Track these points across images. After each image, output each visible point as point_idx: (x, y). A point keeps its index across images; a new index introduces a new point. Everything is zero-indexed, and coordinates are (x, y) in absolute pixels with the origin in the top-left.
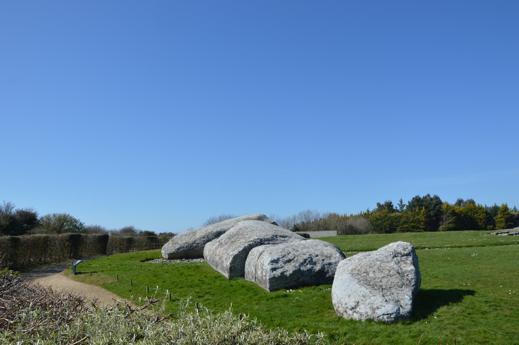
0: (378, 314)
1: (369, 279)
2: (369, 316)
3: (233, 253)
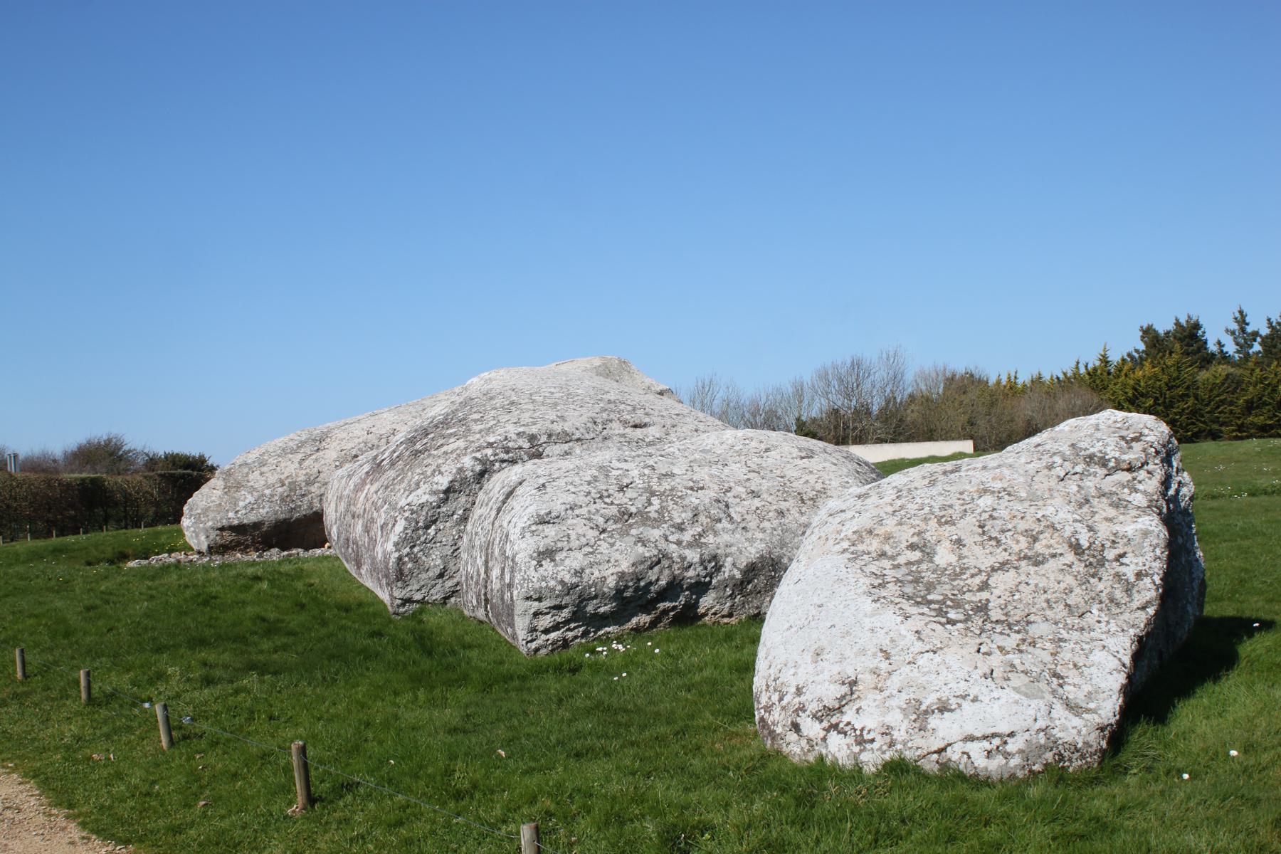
1: (929, 576)
2: (899, 747)
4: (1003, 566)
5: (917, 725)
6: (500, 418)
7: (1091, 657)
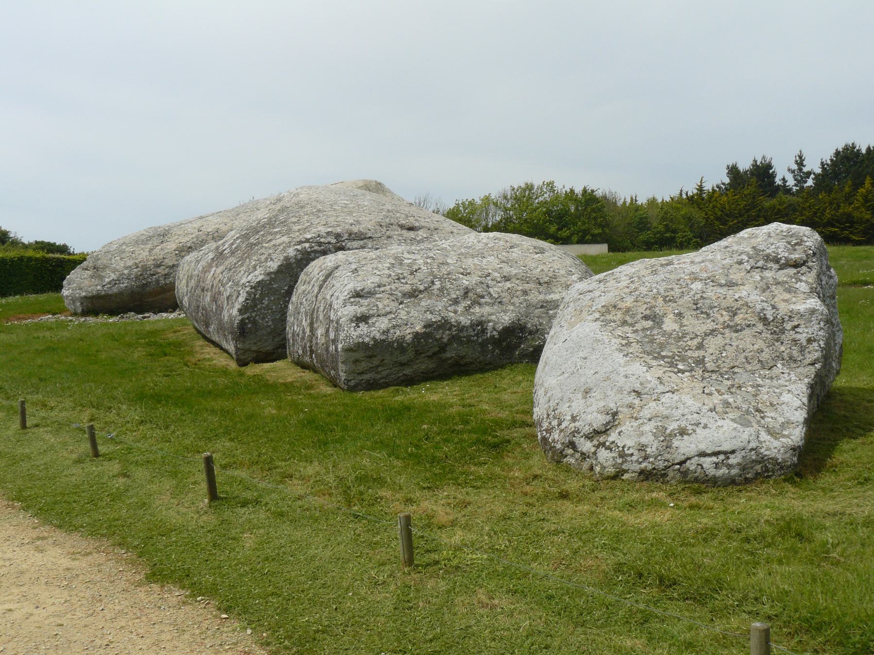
0: (682, 451)
1: (660, 339)
3: (249, 278)
4: (712, 332)
5: (665, 444)
6: (312, 221)
7: (782, 399)
